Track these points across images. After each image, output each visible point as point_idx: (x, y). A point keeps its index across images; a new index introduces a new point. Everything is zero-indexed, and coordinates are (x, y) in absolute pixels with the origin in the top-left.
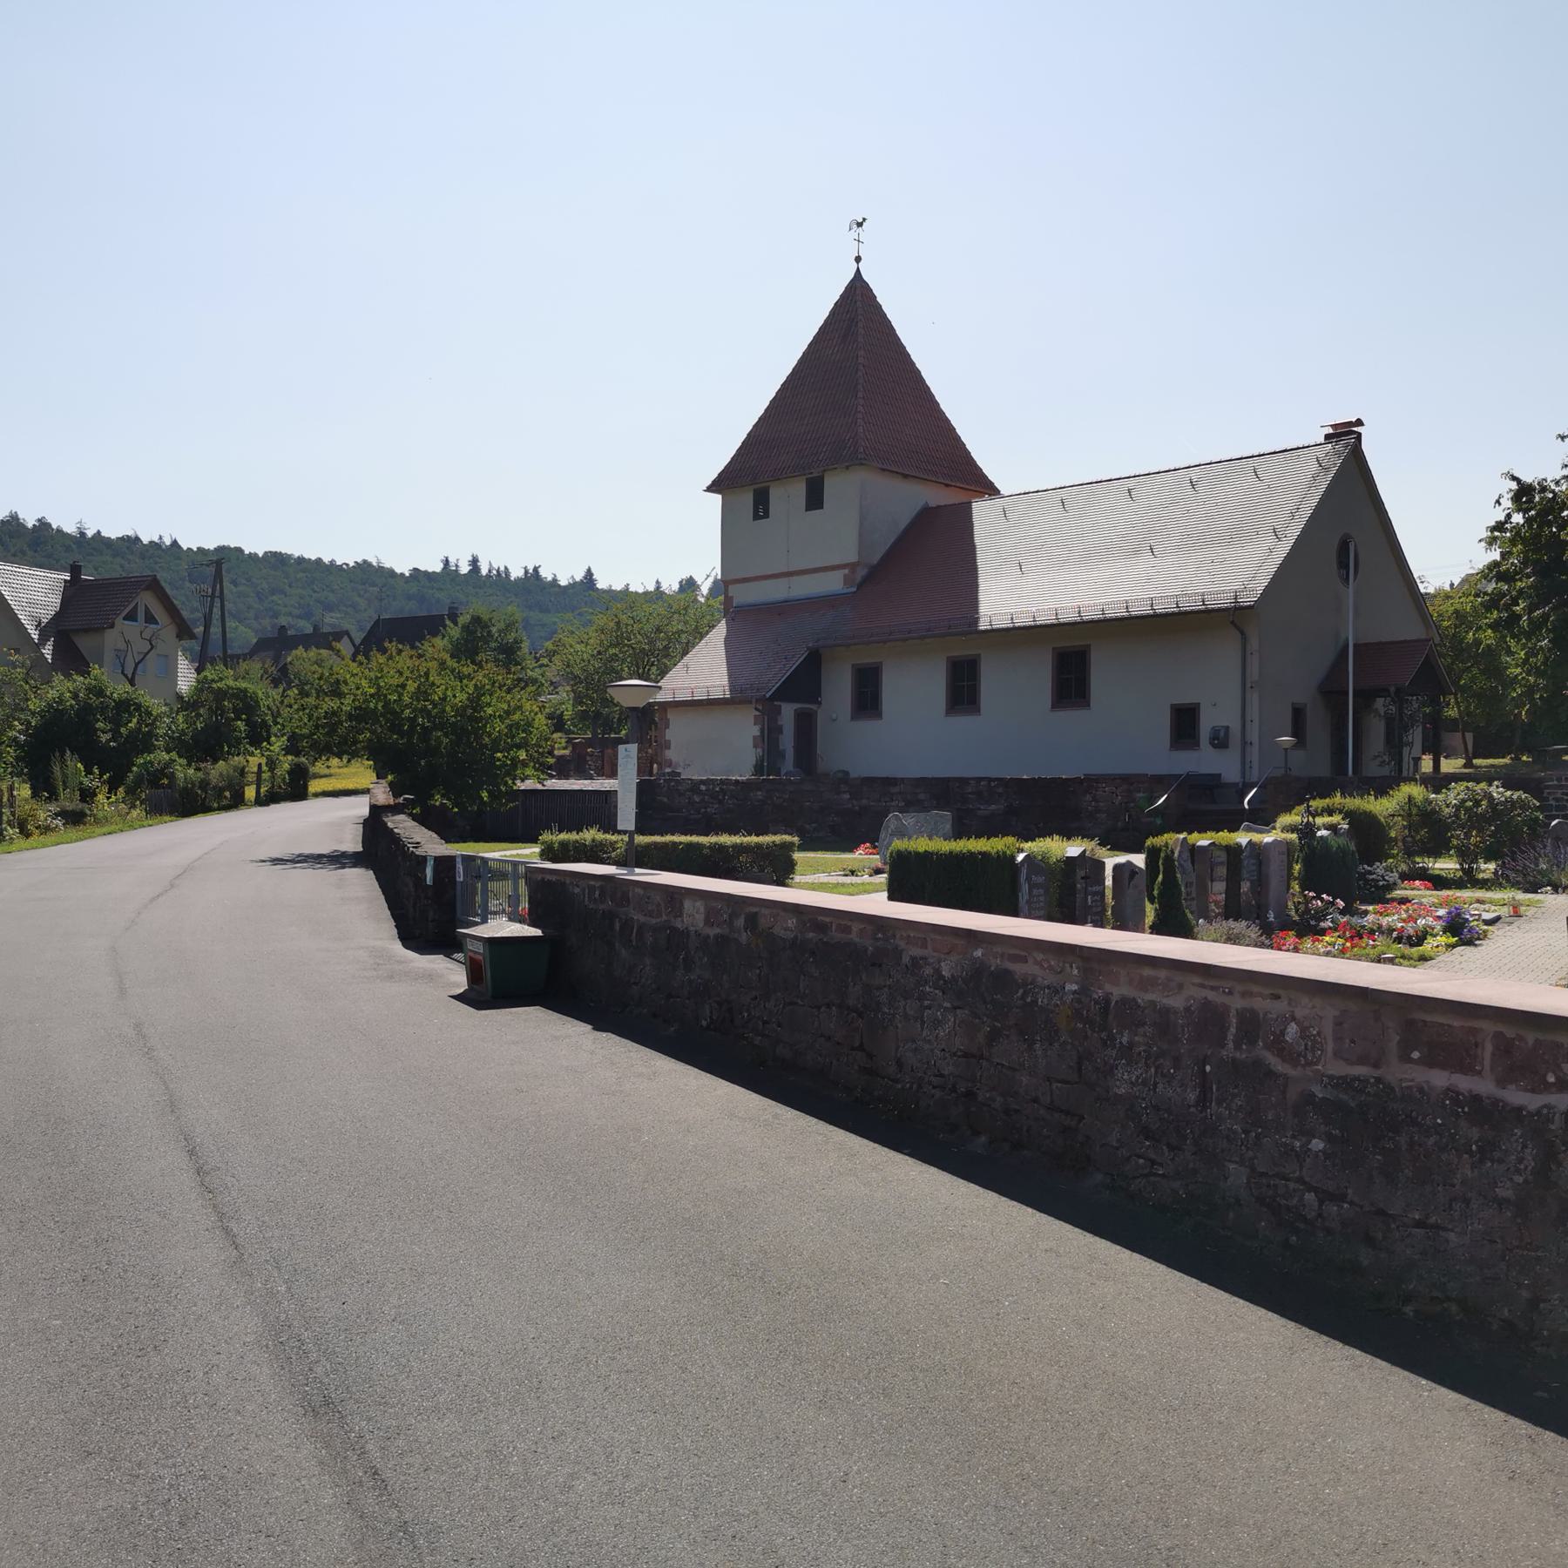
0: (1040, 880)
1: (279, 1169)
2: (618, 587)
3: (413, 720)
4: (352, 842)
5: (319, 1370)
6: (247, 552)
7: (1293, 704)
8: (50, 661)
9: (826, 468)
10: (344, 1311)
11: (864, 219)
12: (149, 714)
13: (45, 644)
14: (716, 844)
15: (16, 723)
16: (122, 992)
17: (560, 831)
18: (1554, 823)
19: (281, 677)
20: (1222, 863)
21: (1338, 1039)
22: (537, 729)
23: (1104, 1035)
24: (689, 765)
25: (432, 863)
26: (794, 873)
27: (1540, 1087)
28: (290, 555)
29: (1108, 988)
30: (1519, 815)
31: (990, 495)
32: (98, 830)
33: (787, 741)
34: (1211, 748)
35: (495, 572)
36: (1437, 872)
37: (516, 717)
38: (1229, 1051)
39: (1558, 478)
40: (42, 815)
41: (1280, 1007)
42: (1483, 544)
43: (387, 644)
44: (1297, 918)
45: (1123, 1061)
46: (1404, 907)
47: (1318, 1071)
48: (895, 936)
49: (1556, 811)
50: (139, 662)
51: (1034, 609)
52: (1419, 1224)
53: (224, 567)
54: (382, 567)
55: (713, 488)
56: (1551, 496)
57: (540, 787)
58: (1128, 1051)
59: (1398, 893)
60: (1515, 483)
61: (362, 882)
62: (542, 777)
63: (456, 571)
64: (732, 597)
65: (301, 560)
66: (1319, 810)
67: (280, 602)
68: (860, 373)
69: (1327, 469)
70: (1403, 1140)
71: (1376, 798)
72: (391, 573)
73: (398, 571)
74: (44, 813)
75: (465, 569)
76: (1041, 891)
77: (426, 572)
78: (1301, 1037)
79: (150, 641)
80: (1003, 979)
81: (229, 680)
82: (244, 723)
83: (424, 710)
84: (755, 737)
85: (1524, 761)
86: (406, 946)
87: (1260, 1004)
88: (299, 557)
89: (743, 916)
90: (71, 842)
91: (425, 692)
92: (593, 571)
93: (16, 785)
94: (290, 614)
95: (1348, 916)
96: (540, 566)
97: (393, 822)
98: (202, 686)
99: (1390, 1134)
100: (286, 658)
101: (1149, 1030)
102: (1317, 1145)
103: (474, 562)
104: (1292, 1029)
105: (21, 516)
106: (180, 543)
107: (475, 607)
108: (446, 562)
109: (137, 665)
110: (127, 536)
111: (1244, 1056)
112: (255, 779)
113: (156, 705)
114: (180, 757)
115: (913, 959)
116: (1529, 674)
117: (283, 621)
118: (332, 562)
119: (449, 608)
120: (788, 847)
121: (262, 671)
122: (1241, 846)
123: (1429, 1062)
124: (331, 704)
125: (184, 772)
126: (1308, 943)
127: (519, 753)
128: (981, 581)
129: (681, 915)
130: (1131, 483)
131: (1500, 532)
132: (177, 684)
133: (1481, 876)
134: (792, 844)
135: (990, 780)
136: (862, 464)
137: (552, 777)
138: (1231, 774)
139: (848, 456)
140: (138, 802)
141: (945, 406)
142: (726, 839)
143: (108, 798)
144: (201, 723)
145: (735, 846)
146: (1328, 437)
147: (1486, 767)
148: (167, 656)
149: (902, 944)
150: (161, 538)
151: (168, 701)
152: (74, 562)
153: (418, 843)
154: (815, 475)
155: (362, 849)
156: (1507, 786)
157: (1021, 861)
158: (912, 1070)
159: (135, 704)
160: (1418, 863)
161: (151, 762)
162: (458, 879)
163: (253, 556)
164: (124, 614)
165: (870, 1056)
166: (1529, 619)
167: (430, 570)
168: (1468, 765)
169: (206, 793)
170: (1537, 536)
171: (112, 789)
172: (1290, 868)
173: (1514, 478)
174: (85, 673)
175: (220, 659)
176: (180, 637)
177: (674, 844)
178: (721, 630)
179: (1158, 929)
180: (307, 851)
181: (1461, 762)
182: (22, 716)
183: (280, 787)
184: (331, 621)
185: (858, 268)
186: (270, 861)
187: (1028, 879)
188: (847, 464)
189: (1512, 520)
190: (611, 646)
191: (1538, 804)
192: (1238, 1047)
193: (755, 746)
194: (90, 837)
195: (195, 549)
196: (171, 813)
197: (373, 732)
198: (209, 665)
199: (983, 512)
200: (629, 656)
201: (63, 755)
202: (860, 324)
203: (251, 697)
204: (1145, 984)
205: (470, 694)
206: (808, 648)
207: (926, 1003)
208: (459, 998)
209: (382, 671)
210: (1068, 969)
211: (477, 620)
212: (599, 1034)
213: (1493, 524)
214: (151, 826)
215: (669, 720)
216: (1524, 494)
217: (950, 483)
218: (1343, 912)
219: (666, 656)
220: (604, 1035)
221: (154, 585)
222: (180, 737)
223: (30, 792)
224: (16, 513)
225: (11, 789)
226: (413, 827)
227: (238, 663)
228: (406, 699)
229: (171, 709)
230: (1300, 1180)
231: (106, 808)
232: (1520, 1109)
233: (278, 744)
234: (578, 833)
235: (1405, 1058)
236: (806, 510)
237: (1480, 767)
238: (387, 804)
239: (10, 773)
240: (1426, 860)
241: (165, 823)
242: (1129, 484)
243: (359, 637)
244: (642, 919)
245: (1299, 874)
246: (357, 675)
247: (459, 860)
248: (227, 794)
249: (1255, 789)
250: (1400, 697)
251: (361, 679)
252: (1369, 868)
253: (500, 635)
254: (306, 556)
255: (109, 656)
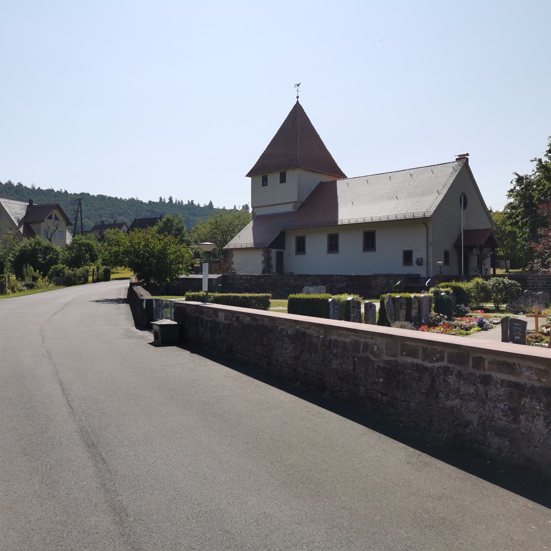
0: (337, 307)
1: (87, 389)
2: (221, 207)
3: (143, 255)
4: (124, 295)
5: (92, 437)
6: (91, 195)
7: (444, 250)
8: (22, 233)
9: (287, 168)
10: (101, 424)
11: (300, 84)
12: (56, 251)
13: (20, 227)
14: (244, 296)
15: (11, 254)
16: (43, 341)
17: (192, 292)
18: (525, 291)
19: (102, 239)
20: (404, 303)
21: (386, 350)
22: (186, 257)
23: (330, 351)
24: (240, 270)
25: (145, 301)
26: (270, 306)
27: (432, 361)
28: (106, 196)
29: (331, 336)
30: (514, 288)
31: (343, 178)
32: (38, 291)
33: (274, 262)
34: (416, 265)
35: (178, 202)
36: (487, 308)
37: (178, 253)
38: (361, 354)
39: (531, 175)
40: (19, 285)
41: (373, 341)
42: (507, 196)
43: (134, 229)
44: (432, 322)
45: (335, 358)
46: (468, 318)
47: (381, 359)
48: (276, 322)
49: (531, 287)
50: (53, 233)
51: (356, 218)
52: (405, 401)
53: (82, 201)
54: (139, 200)
55: (249, 175)
56: (529, 180)
57: (187, 277)
58: (335, 355)
59: (469, 314)
60: (517, 176)
61: (125, 308)
62: (188, 273)
63: (164, 202)
64: (255, 213)
65: (110, 198)
66: (444, 286)
67: (103, 212)
68: (298, 137)
69: (456, 171)
70: (401, 377)
71: (467, 282)
72: (141, 202)
73: (144, 202)
74: (19, 285)
75: (167, 201)
76: (338, 311)
77: (154, 202)
78: (377, 349)
79: (56, 226)
80: (304, 334)
81: (84, 240)
82: (89, 255)
83: (147, 251)
84: (262, 261)
85: (526, 271)
86: (137, 328)
87: (369, 340)
88: (109, 197)
89: (235, 317)
90: (29, 295)
91: (148, 245)
92: (212, 202)
93: (10, 275)
94: (106, 217)
95: (448, 321)
96: (193, 200)
97: (135, 288)
98: (74, 242)
99: (398, 376)
100: (104, 232)
101: (341, 349)
102: (381, 380)
103: (171, 199)
104: (376, 347)
105: (12, 182)
106: (68, 192)
107: (168, 216)
108: (161, 199)
109: (52, 235)
110: (49, 189)
111: (364, 355)
112: (92, 274)
113: (58, 248)
114: (67, 266)
115: (281, 329)
116: (523, 241)
117: (104, 219)
118: (121, 198)
119: (160, 215)
120: (268, 298)
121: (95, 237)
122: (411, 298)
123: (408, 355)
124: (115, 249)
125: (68, 271)
126: (431, 329)
127: (180, 265)
128: (339, 208)
129: (218, 317)
130: (390, 175)
131: (512, 192)
132: (66, 241)
133: (501, 309)
134: (269, 296)
135: (341, 276)
136: (299, 167)
137: (192, 274)
138: (423, 274)
139: (295, 166)
140: (52, 282)
141: (328, 148)
142: (247, 295)
143: (42, 280)
144: (74, 255)
145: (250, 297)
146: (457, 159)
147: (513, 272)
148: (62, 231)
149: (278, 325)
150: (61, 190)
151: (62, 247)
152: (30, 199)
153: (142, 295)
154: (283, 171)
155: (127, 298)
156: (509, 279)
157: (331, 301)
158: (280, 363)
159: (51, 248)
160: (480, 304)
161: (56, 268)
162: (154, 307)
163: (93, 196)
164: (47, 217)
165: (269, 359)
166: (522, 222)
167: (155, 202)
168: (507, 271)
169: (75, 278)
170: (525, 194)
171: (44, 276)
172: (430, 306)
173: (517, 174)
174: (34, 237)
175: (81, 233)
176: (67, 225)
177: (230, 296)
178: (251, 224)
179: (379, 324)
180: (108, 298)
181: (505, 270)
182: (13, 252)
183: (101, 277)
184: (120, 219)
185: (298, 100)
186: (96, 301)
187: (333, 307)
188: (293, 167)
189: (516, 189)
190: (214, 229)
191: (520, 285)
192: (363, 353)
193: (263, 264)
194: (36, 293)
195: (73, 194)
196: (63, 285)
197: (130, 258)
198: (76, 235)
199: (340, 184)
200: (220, 233)
201: (27, 265)
202: (298, 120)
203: (91, 246)
204: (340, 335)
205: (162, 246)
206: (281, 230)
207: (284, 342)
208: (151, 344)
209: (133, 237)
210: (321, 331)
211: (168, 220)
212: (192, 354)
213: (510, 190)
214: (56, 289)
215: (233, 254)
216: (520, 180)
217: (329, 174)
218: (447, 320)
219: (233, 232)
220: (194, 354)
221: (58, 207)
222: (66, 259)
223: (15, 278)
224: (10, 181)
225: (9, 277)
226: (142, 290)
227: (87, 234)
228: (141, 247)
229: (64, 250)
230: (377, 390)
231: (41, 283)
232: (427, 367)
233: (99, 261)
234: (198, 292)
235: (402, 355)
236: (280, 183)
237: (511, 272)
238: (135, 282)
239: (9, 271)
240: (483, 304)
241: (61, 288)
242: (390, 175)
243: (129, 224)
244: (207, 318)
245: (434, 307)
246: (124, 239)
247: (154, 300)
248: (83, 279)
249: (430, 279)
250: (481, 248)
251: (126, 241)
252: (460, 306)
253: (176, 225)
254: (112, 196)
255: (42, 232)
